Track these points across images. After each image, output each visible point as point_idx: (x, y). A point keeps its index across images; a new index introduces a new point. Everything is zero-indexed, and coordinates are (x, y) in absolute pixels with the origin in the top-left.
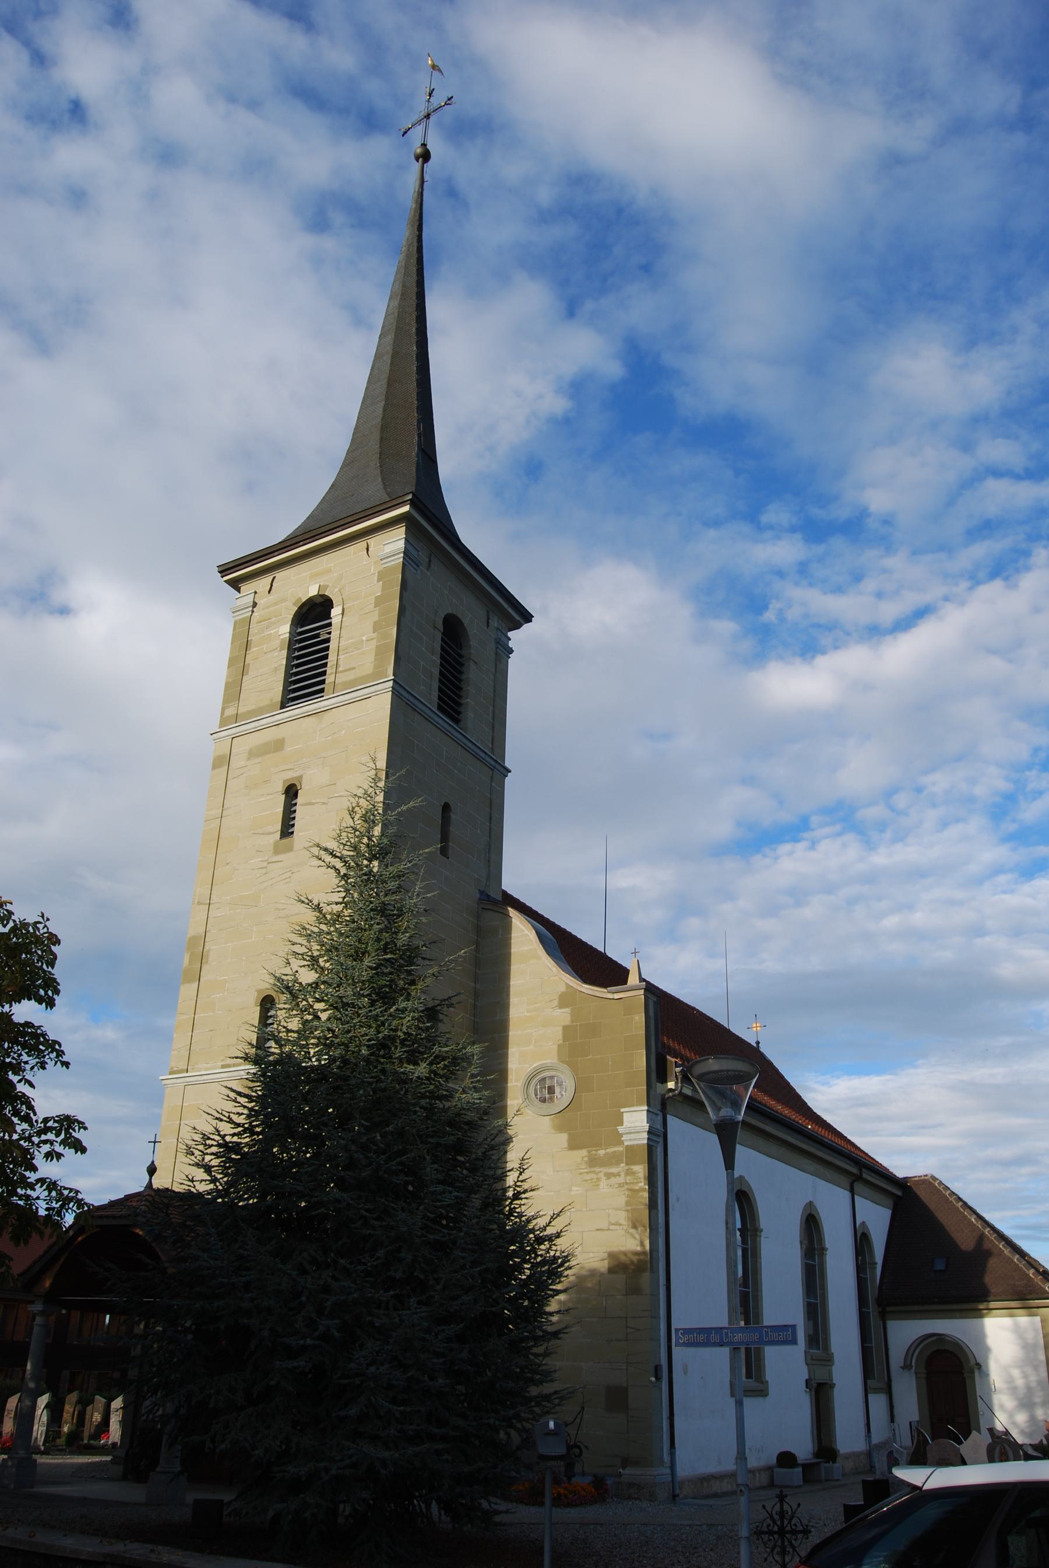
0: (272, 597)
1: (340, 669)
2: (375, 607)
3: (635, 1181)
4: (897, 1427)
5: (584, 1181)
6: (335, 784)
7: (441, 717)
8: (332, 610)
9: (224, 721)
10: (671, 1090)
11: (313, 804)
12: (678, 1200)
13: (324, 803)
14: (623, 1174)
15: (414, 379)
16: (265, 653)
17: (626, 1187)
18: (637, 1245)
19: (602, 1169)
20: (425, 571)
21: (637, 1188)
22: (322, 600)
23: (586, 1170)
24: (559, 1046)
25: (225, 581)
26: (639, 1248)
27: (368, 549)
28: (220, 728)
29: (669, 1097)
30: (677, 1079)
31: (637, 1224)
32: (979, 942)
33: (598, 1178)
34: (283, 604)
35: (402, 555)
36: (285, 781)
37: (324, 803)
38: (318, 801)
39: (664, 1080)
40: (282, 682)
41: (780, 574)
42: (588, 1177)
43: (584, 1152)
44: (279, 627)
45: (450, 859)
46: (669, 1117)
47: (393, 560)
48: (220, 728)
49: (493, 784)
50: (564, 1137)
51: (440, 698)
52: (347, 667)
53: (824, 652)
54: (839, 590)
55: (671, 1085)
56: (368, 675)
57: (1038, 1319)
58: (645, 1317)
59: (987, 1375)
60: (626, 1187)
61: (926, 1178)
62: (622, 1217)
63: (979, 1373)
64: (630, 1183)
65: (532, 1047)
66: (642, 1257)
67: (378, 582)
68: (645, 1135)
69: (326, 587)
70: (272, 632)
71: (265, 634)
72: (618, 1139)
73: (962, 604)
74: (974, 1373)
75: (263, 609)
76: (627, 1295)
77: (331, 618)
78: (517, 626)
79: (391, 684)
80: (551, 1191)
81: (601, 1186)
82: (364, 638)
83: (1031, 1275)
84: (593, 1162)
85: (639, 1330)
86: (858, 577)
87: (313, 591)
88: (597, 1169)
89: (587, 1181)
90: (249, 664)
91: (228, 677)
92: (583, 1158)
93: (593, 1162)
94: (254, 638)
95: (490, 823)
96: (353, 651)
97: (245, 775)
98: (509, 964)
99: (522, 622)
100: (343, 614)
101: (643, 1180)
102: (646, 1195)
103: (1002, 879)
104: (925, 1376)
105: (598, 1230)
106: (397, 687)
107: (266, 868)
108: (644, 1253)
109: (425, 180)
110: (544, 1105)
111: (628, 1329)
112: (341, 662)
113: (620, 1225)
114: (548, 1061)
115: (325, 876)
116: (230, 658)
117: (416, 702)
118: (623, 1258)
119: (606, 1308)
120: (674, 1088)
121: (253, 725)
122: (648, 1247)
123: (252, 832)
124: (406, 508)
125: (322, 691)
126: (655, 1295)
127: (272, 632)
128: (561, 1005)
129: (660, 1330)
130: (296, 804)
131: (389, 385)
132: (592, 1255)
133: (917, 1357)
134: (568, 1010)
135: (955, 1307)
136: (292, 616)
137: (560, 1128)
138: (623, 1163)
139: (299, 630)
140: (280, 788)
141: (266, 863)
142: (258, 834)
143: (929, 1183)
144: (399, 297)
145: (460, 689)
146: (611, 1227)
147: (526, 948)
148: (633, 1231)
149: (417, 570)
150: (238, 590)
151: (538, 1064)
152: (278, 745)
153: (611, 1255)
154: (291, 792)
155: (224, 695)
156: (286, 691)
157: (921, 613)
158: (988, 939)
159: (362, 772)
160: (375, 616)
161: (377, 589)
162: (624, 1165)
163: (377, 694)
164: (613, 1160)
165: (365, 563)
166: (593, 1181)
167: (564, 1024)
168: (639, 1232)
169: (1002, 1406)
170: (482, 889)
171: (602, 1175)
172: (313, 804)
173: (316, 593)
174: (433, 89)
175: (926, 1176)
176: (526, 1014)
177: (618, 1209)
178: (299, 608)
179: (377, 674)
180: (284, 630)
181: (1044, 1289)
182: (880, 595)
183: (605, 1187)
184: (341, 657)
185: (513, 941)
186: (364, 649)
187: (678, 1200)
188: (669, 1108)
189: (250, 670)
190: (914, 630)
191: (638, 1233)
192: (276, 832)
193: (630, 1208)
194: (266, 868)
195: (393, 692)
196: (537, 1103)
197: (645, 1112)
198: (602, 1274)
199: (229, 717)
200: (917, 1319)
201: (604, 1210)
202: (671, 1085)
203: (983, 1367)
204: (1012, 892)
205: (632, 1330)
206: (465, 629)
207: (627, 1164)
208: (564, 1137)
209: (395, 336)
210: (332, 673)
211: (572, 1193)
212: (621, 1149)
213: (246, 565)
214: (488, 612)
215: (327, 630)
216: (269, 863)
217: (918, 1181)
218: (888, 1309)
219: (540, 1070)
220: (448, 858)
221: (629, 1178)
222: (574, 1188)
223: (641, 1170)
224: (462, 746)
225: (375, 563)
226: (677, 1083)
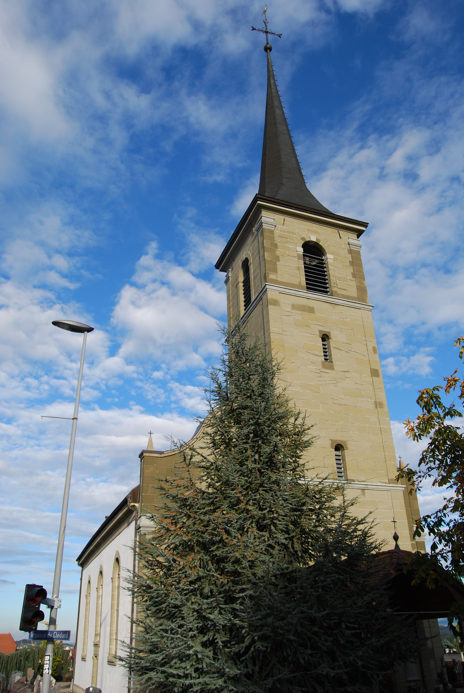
11: (341, 350)
13: (347, 352)
37: (347, 352)
172: (341, 350)
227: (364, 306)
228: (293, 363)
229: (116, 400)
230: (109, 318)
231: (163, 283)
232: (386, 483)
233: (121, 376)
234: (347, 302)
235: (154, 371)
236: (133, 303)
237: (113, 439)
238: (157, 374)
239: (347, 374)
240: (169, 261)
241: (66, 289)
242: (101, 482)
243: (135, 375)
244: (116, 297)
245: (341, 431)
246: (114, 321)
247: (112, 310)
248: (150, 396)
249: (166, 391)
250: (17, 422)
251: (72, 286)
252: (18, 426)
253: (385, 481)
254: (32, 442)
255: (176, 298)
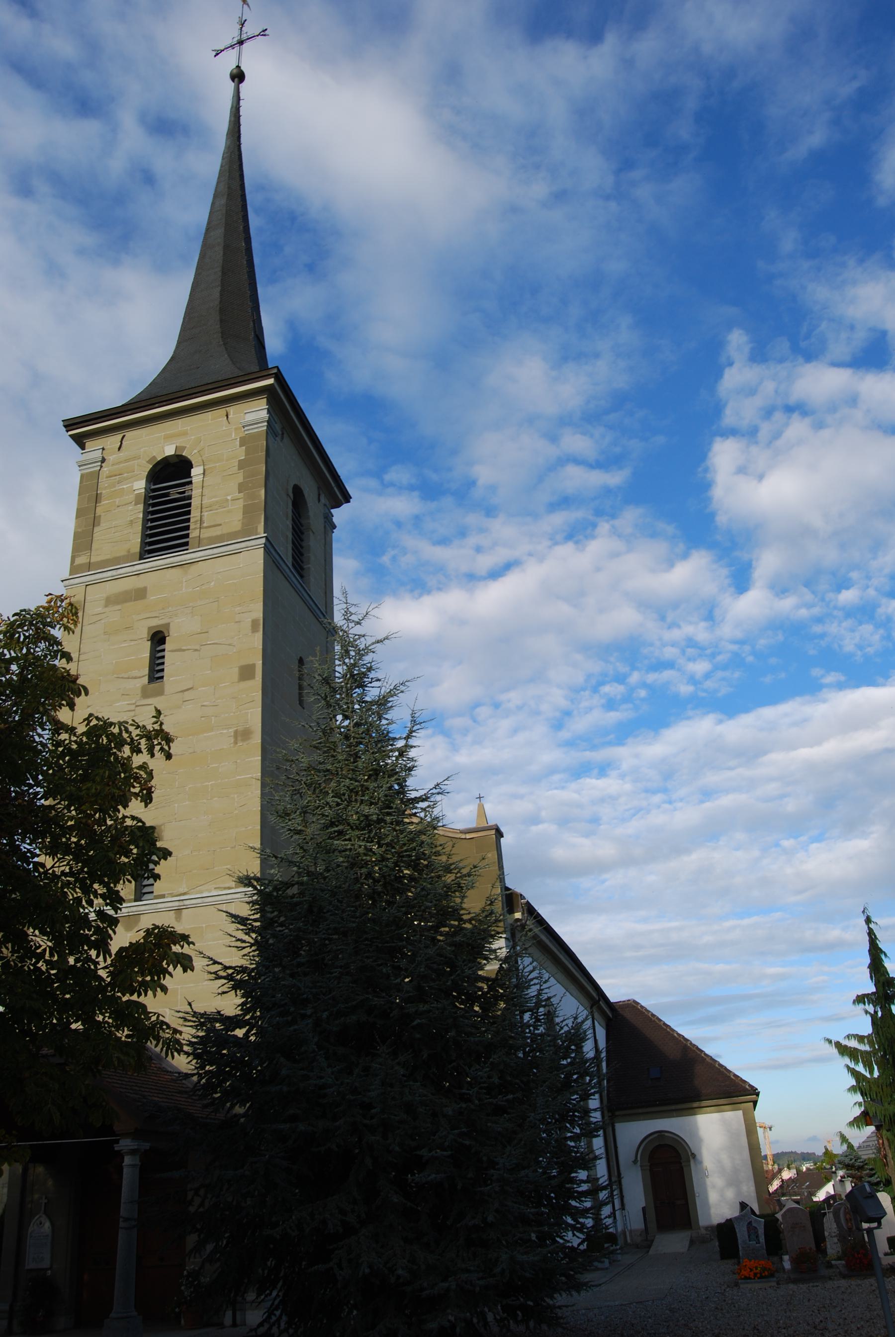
0: (122, 454)
1: (205, 525)
2: (239, 470)
4: (627, 1214)
6: (207, 632)
7: (296, 578)
8: (192, 470)
9: (75, 569)
10: (518, 920)
11: (184, 650)
13: (196, 650)
16: (118, 506)
22: (176, 460)
25: (70, 436)
27: (227, 416)
28: (70, 575)
32: (534, 829)
34: (136, 461)
35: (266, 424)
36: (150, 628)
37: (196, 650)
38: (189, 647)
40: (140, 534)
41: (399, 524)
44: (133, 483)
47: (256, 428)
48: (70, 575)
52: (212, 524)
53: (429, 592)
54: (444, 541)
56: (236, 532)
57: (740, 1112)
59: (701, 1163)
61: (629, 1002)
63: (695, 1162)
67: (240, 446)
69: (184, 448)
70: (125, 487)
71: (117, 488)
73: (541, 559)
74: (690, 1161)
75: (113, 465)
77: (191, 477)
78: (338, 505)
79: (263, 541)
83: (732, 1077)
86: (462, 533)
87: (170, 451)
90: (100, 516)
91: (76, 527)
94: (104, 492)
96: (217, 509)
97: (103, 621)
99: (343, 502)
100: (204, 474)
103: (556, 777)
104: (649, 1168)
107: (134, 710)
109: (241, 98)
112: (205, 518)
115: (203, 719)
116: (77, 509)
117: (281, 562)
120: (520, 918)
121: (110, 574)
123: (115, 676)
124: (271, 381)
125: (187, 544)
127: (125, 487)
130: (164, 650)
131: (224, 273)
133: (642, 1152)
135: (673, 1107)
136: (147, 473)
139: (153, 487)
140: (145, 634)
141: (134, 706)
142: (122, 678)
143: (632, 1006)
144: (226, 197)
150: (83, 447)
152: (140, 594)
154: (158, 639)
155: (73, 544)
156: (144, 544)
157: (507, 567)
158: (541, 827)
159: (237, 622)
160: (240, 478)
161: (241, 453)
163: (248, 549)
165: (224, 428)
169: (714, 1187)
172: (184, 650)
173: (173, 453)
174: (246, 20)
175: (629, 1000)
178: (154, 466)
179: (247, 531)
180: (140, 485)
181: (745, 1088)
182: (479, 549)
184: (205, 514)
186: (230, 508)
189: (102, 521)
190: (500, 579)
192: (143, 676)
194: (134, 710)
195: (265, 549)
199: (80, 566)
200: (640, 1120)
203: (698, 1157)
204: (563, 788)
209: (225, 230)
210: (195, 529)
213: (105, 419)
215: (187, 487)
216: (137, 706)
217: (623, 1005)
218: (617, 1113)
225: (236, 429)
226: (523, 914)
227: (248, 542)
228: (89, 707)
229: (783, 675)
230: (712, 516)
231: (790, 409)
232: (229, 888)
233: (776, 625)
234: (211, 550)
235: (839, 592)
236: (742, 470)
237: (804, 753)
238: (848, 596)
239: (188, 695)
240: (781, 361)
241: (607, 491)
242: (812, 843)
243: (803, 612)
244: (706, 470)
245: (156, 809)
246: (721, 519)
247: (709, 500)
248: (849, 646)
249: (877, 626)
250: (619, 769)
251: (615, 478)
252: (622, 776)
253: (227, 885)
254: (657, 798)
255: (826, 433)
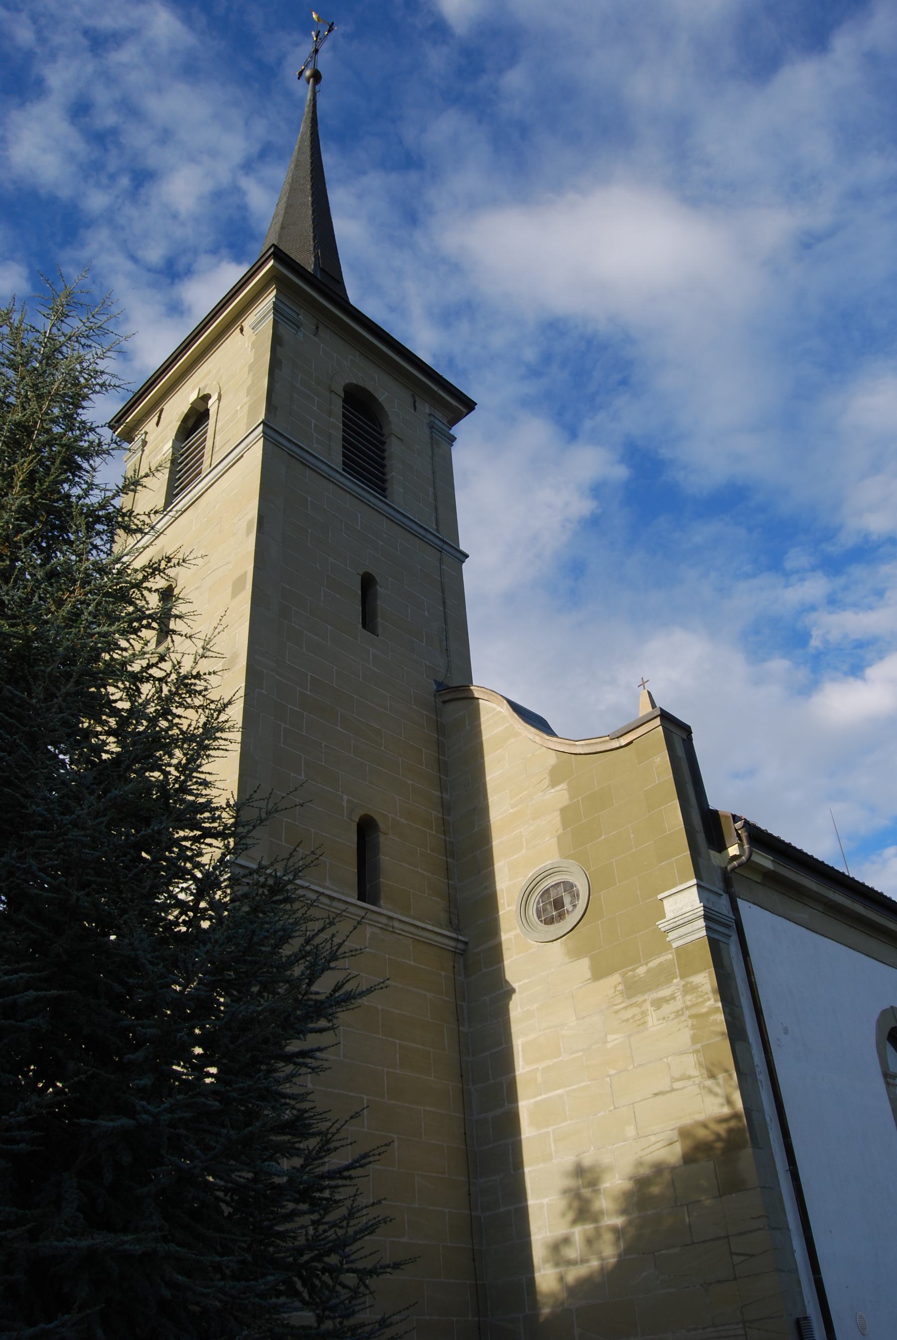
3: (700, 1000)
5: (624, 1021)
10: (735, 858)
12: (786, 1031)
14: (679, 995)
15: (310, 219)
17: (687, 1013)
18: (723, 1105)
19: (646, 997)
20: (312, 337)
21: (704, 1010)
23: (624, 1005)
24: (559, 837)
26: (726, 1110)
29: (734, 869)
30: (740, 839)
31: (716, 1070)
33: (642, 1013)
39: (721, 847)
42: (628, 1014)
43: (616, 978)
45: (380, 637)
46: (740, 902)
49: (443, 567)
50: (584, 964)
51: (344, 455)
55: (733, 850)
58: (759, 1229)
60: (687, 1013)
62: (690, 1064)
64: (693, 1006)
65: (524, 851)
66: (733, 1124)
68: (701, 923)
72: (660, 941)
76: (720, 1196)
80: (577, 1052)
81: (650, 1024)
82: (238, 408)
84: (632, 989)
85: (753, 1256)
88: (639, 998)
89: (627, 1020)
92: (615, 987)
93: (632, 989)
95: (444, 608)
98: (482, 757)
101: (711, 995)
102: (721, 1017)
105: (656, 1094)
106: (270, 432)
108: (735, 1116)
110: (551, 927)
111: (734, 1257)
113: (690, 1077)
114: (548, 863)
118: (702, 1133)
119: (690, 1225)
120: (738, 853)
122: (739, 1105)
126: (770, 1188)
128: (554, 784)
129: (793, 1252)
132: (653, 1139)
134: (563, 786)
137: (576, 953)
138: (676, 977)
145: (384, 466)
146: (676, 1085)
147: (500, 729)
148: (709, 1083)
149: (297, 331)
151: (532, 873)
153: (684, 1133)
162: (679, 979)
164: (661, 977)
166: (637, 1018)
167: (560, 806)
168: (721, 1081)
170: (440, 680)
171: (647, 1006)
176: (511, 811)
177: (681, 1053)
183: (656, 1023)
185: (483, 727)
187: (786, 1031)
188: (737, 888)
191: (718, 1084)
193: (699, 1046)
195: (264, 438)
196: (542, 926)
197: (695, 889)
198: (673, 1169)
201: (661, 1059)
202: (733, 850)
205: (742, 1258)
206: (382, 408)
207: (682, 978)
208: (584, 964)
211: (609, 1046)
212: (670, 956)
214: (413, 396)
219: (538, 879)
220: (378, 636)
221: (688, 997)
222: (610, 1038)
223: (706, 980)
224: (387, 517)
226: (741, 846)
